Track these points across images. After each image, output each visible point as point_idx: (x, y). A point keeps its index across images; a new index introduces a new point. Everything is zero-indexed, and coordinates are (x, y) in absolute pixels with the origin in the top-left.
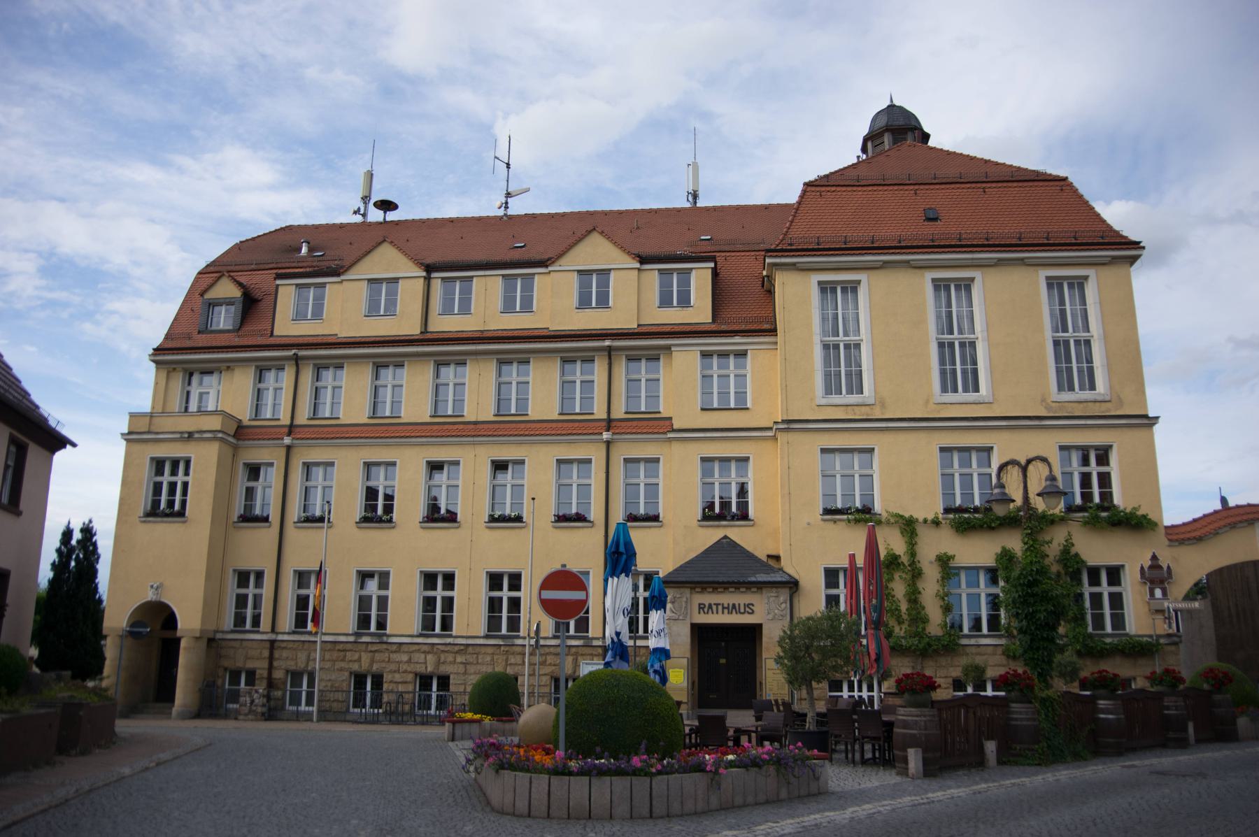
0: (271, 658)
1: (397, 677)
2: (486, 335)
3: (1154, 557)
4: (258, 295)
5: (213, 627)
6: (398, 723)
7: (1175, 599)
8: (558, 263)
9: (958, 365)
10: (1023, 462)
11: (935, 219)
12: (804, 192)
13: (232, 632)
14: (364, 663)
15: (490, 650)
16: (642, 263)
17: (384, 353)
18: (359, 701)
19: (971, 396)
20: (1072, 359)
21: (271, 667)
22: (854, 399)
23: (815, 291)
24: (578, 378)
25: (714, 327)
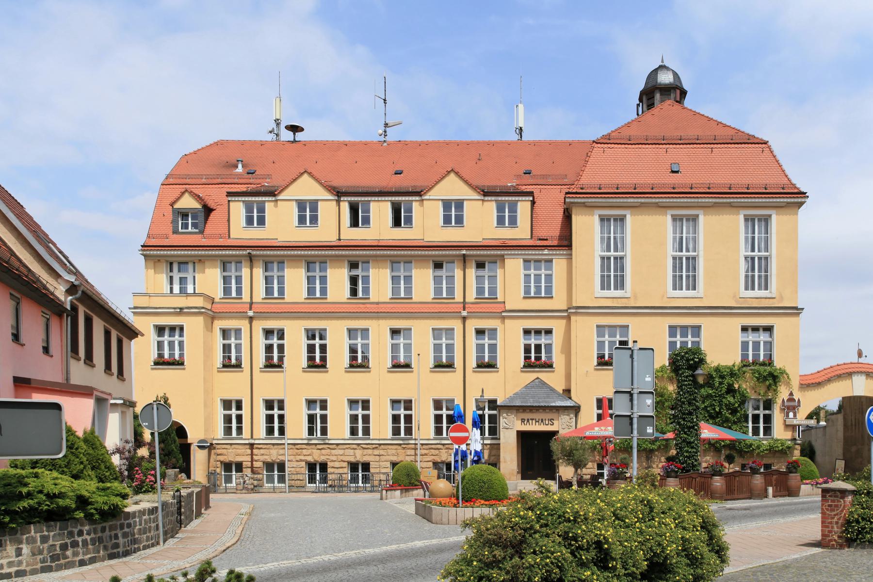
1: (337, 464)
4: (211, 204)
7: (801, 418)
8: (429, 194)
9: (685, 270)
11: (677, 172)
14: (359, 456)
18: (312, 479)
19: (691, 293)
20: (758, 271)
22: (619, 293)
24: (402, 274)
25: (531, 243)
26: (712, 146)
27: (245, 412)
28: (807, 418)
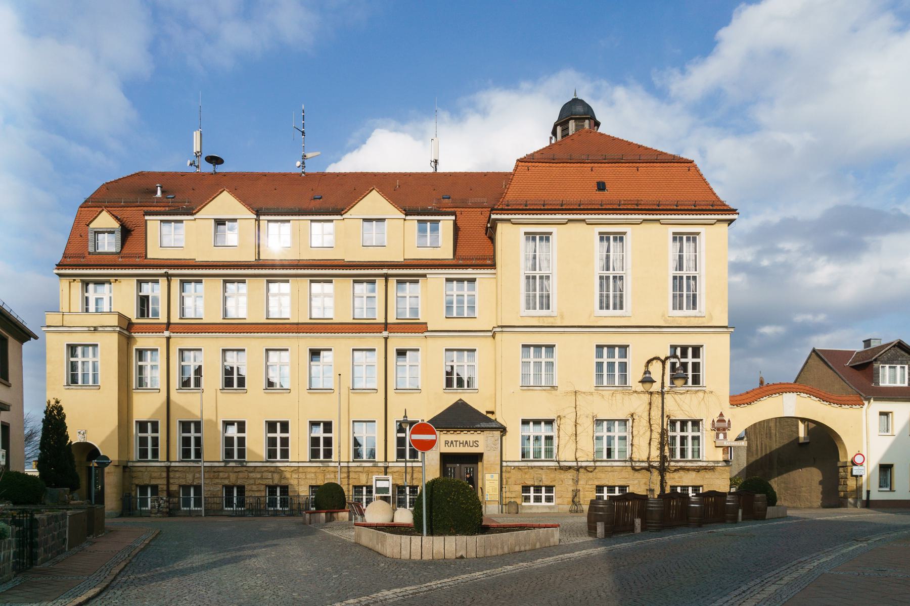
0: (168, 477)
1: (255, 488)
2: (301, 263)
3: (721, 415)
5: (125, 459)
6: (260, 516)
7: (731, 438)
9: (611, 292)
10: (663, 358)
12: (517, 166)
13: (139, 461)
14: (232, 479)
15: (313, 470)
16: (406, 215)
17: (232, 272)
21: (168, 484)
23: (523, 237)
25: (454, 262)
26: (638, 165)
27: (161, 435)
28: (737, 440)
